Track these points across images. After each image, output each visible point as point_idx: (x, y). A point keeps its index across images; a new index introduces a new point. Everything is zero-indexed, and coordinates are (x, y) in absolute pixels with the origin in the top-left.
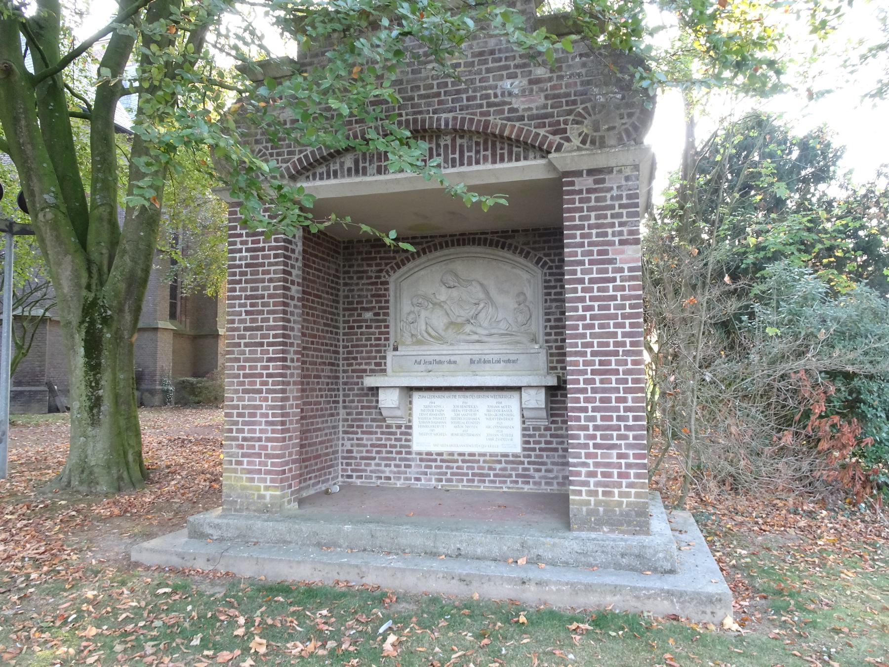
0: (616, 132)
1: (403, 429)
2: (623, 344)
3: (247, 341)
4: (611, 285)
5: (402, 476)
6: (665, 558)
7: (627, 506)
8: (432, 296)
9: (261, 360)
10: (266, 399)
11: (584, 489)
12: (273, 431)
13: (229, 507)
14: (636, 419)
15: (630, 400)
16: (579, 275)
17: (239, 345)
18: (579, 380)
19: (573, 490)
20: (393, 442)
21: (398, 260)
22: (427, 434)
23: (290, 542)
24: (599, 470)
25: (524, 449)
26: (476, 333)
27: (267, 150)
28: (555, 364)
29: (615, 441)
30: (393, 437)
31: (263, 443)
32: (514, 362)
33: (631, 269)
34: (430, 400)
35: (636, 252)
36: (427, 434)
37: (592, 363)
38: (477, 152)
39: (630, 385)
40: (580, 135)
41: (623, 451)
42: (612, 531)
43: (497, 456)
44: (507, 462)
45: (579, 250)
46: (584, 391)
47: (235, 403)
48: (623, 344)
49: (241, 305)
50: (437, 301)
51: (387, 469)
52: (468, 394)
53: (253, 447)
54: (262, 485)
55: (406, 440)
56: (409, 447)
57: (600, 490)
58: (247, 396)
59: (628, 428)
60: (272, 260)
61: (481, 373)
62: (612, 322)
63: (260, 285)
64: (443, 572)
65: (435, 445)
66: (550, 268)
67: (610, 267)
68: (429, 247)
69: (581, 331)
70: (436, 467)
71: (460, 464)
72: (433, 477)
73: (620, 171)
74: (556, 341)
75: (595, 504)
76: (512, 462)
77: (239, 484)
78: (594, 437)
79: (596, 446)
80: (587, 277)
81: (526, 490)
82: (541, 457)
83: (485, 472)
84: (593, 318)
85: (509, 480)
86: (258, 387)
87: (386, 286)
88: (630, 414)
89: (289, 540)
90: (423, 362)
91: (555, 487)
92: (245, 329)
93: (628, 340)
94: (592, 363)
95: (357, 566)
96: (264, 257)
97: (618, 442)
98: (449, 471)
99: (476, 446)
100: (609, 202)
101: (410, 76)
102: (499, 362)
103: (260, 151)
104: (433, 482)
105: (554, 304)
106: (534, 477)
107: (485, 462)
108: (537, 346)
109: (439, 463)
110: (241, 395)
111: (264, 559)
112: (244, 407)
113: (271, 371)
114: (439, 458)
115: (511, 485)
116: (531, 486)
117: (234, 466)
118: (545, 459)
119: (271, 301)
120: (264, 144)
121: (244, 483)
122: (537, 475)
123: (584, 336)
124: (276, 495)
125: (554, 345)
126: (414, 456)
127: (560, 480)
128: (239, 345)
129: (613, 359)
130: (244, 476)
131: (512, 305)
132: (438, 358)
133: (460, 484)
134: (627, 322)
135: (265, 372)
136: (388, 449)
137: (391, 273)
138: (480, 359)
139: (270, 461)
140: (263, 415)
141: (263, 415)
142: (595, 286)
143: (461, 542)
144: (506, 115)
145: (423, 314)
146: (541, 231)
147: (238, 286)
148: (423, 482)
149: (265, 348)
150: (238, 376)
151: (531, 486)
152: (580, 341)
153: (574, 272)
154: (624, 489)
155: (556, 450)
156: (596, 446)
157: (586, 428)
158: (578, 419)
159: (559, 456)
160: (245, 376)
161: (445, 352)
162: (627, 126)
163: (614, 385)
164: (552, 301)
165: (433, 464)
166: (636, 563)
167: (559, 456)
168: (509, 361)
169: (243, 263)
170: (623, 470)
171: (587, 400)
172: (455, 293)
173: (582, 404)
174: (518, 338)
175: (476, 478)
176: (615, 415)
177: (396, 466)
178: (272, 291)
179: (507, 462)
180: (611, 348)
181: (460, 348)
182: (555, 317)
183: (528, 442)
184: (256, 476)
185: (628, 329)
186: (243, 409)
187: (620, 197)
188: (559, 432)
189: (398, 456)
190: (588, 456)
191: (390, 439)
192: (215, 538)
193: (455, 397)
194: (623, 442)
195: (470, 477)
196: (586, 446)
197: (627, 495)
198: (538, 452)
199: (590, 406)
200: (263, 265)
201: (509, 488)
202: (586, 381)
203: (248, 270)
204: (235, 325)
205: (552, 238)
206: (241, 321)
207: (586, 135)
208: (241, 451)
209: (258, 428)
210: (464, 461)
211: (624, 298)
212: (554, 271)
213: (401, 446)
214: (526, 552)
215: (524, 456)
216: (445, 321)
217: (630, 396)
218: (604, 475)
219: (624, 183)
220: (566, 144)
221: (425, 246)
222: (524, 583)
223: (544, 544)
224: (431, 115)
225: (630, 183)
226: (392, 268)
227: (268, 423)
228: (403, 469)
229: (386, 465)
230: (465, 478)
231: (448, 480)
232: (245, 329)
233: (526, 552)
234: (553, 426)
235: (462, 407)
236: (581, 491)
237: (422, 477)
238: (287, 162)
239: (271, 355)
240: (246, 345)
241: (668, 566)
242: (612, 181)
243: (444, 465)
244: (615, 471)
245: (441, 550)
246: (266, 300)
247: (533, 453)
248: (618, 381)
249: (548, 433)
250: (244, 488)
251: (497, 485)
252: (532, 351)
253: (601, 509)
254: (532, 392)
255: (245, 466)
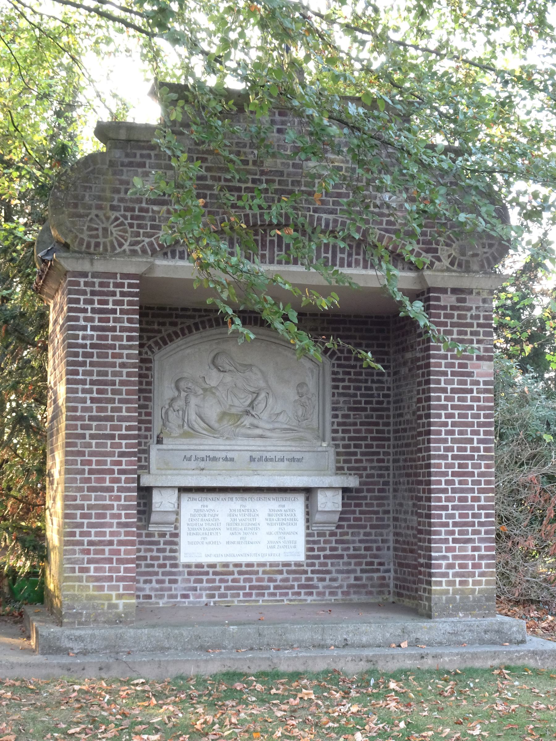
0: (479, 258)
1: (168, 538)
2: (478, 450)
3: (93, 432)
4: (469, 396)
5: (166, 593)
6: (518, 631)
7: (479, 593)
8: (201, 380)
9: (112, 454)
10: (118, 498)
11: (444, 580)
12: (127, 534)
13: (71, 620)
14: (487, 515)
15: (483, 499)
16: (443, 385)
17: (83, 436)
18: (441, 481)
19: (436, 582)
20: (155, 554)
21: (164, 334)
22: (197, 543)
23: (169, 648)
24: (457, 562)
25: (308, 557)
26: (257, 427)
27: (126, 219)
28: (341, 464)
29: (470, 536)
30: (154, 547)
31: (115, 547)
32: (299, 460)
33: (485, 383)
34: (201, 503)
35: (489, 367)
36: (197, 543)
37: (452, 466)
38: (350, 255)
39: (483, 486)
40: (449, 256)
41: (477, 544)
42: (466, 616)
43: (278, 565)
44: (288, 572)
45: (443, 362)
46: (445, 491)
47: (78, 502)
48: (478, 450)
49: (84, 391)
50: (207, 386)
51: (147, 586)
52: (247, 496)
53: (103, 552)
54: (114, 593)
55: (172, 551)
56: (175, 558)
57: (458, 580)
58: (93, 494)
59: (481, 524)
60: (125, 342)
61: (263, 473)
62: (469, 429)
63: (110, 370)
64: (352, 656)
65: (207, 556)
66: (339, 359)
67: (469, 379)
68: (203, 323)
69: (443, 436)
70: (208, 581)
71: (236, 576)
72: (204, 593)
73: (478, 294)
74: (343, 439)
75: (453, 594)
76: (295, 572)
77: (84, 594)
78: (453, 533)
79: (455, 541)
80: (449, 387)
81: (309, 602)
82: (326, 565)
83: (265, 584)
84: (454, 424)
85: (290, 591)
86: (108, 484)
87: (148, 365)
88: (483, 512)
89: (167, 646)
90: (193, 458)
91: (340, 596)
92: (91, 418)
93: (482, 446)
94: (452, 466)
95: (268, 658)
96: (115, 338)
97: (473, 537)
98: (223, 585)
99: (256, 555)
100: (469, 320)
101: (291, 169)
102: (282, 460)
103: (117, 219)
104: (204, 599)
105: (342, 399)
106: (317, 587)
107: (264, 572)
108: (324, 444)
109: (211, 576)
110: (86, 493)
111: (168, 662)
112: (90, 507)
113: (124, 467)
114: (211, 570)
115: (294, 597)
116: (315, 597)
117: (77, 574)
118: (329, 567)
119: (124, 388)
120: (122, 212)
121: (91, 592)
122: (320, 584)
123: (445, 441)
124: (130, 604)
125: (341, 443)
126: (181, 569)
127: (345, 589)
128: (83, 436)
129: (470, 462)
130: (91, 585)
131: (293, 396)
132: (212, 454)
133: (236, 600)
134: (482, 429)
135: (116, 468)
136: (149, 562)
137: (155, 349)
138: (262, 457)
139: (122, 567)
140: (113, 516)
141: (113, 516)
142: (456, 396)
143: (348, 633)
144: (384, 226)
145: (193, 401)
146: (330, 317)
147: (81, 369)
148: (191, 599)
149: (117, 440)
150: (82, 472)
151: (315, 597)
152: (442, 446)
153: (438, 382)
154: (477, 578)
155: (341, 557)
156: (455, 541)
157: (446, 525)
158: (440, 516)
159: (344, 564)
160: (91, 472)
161: (222, 448)
162: (488, 255)
163: (470, 486)
164: (340, 395)
165: (205, 578)
166: (496, 637)
167: (344, 564)
168: (293, 460)
169: (88, 342)
170: (476, 561)
171: (448, 499)
172: (228, 378)
173: (444, 503)
174: (302, 434)
175: (254, 592)
176: (470, 512)
177: (158, 582)
178: (124, 378)
179: (288, 572)
180: (468, 453)
181: (239, 442)
182: (343, 412)
183: (312, 549)
184: (106, 584)
185: (482, 436)
186: (88, 509)
187: (477, 317)
188: (345, 538)
189: (161, 570)
190: (448, 550)
191: (151, 550)
192: (76, 651)
193: (232, 499)
194: (476, 537)
195: (247, 591)
196: (446, 541)
197: (479, 583)
198: (322, 560)
199: (450, 504)
200: (113, 347)
201: (291, 600)
202: (447, 482)
203: (95, 351)
204: (78, 414)
205: (341, 326)
206: (84, 409)
207: (455, 258)
208: (86, 557)
209: (108, 530)
210: (240, 573)
211: (479, 408)
212: (343, 362)
213: (165, 558)
214: (407, 636)
215: (308, 565)
216: (218, 410)
217: (482, 496)
218: (461, 566)
219: (481, 304)
220: (437, 263)
221: (197, 320)
222: (423, 657)
223: (422, 628)
224: (311, 213)
225: (486, 305)
226: (156, 343)
227: (120, 525)
228: (167, 585)
229: (146, 582)
230: (241, 592)
231: (222, 596)
232: (91, 418)
233: (407, 636)
234: (339, 531)
235: (240, 511)
236: (441, 582)
237: (190, 593)
238: (151, 236)
239: (124, 449)
240: (92, 437)
241: (519, 637)
242: (472, 302)
243: (218, 578)
244: (470, 563)
245: (329, 642)
246: (117, 387)
247: (317, 561)
248: (474, 483)
249: (334, 538)
250: (90, 598)
251: (278, 598)
252: (320, 449)
253: (458, 597)
254: (329, 494)
255: (92, 573)
